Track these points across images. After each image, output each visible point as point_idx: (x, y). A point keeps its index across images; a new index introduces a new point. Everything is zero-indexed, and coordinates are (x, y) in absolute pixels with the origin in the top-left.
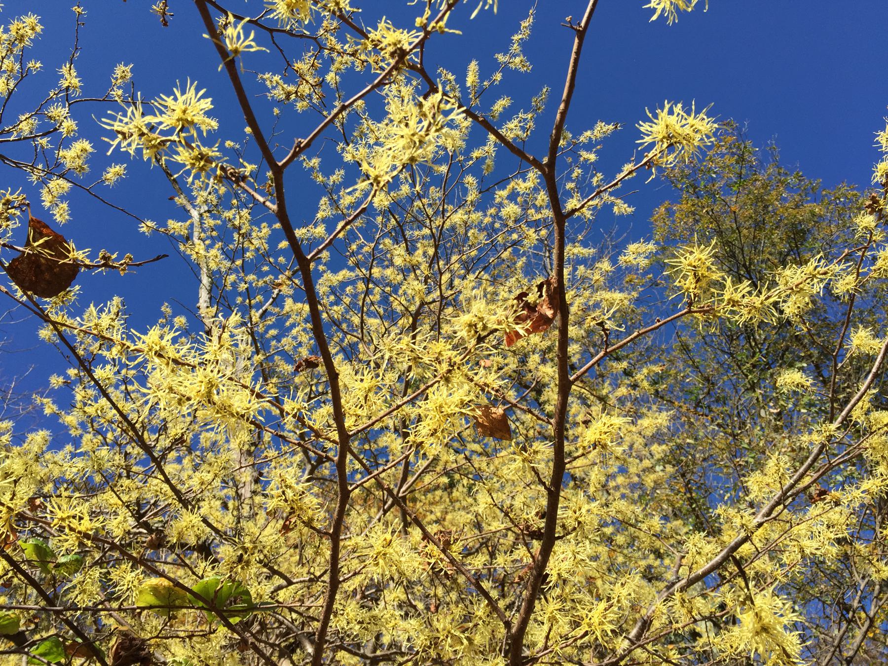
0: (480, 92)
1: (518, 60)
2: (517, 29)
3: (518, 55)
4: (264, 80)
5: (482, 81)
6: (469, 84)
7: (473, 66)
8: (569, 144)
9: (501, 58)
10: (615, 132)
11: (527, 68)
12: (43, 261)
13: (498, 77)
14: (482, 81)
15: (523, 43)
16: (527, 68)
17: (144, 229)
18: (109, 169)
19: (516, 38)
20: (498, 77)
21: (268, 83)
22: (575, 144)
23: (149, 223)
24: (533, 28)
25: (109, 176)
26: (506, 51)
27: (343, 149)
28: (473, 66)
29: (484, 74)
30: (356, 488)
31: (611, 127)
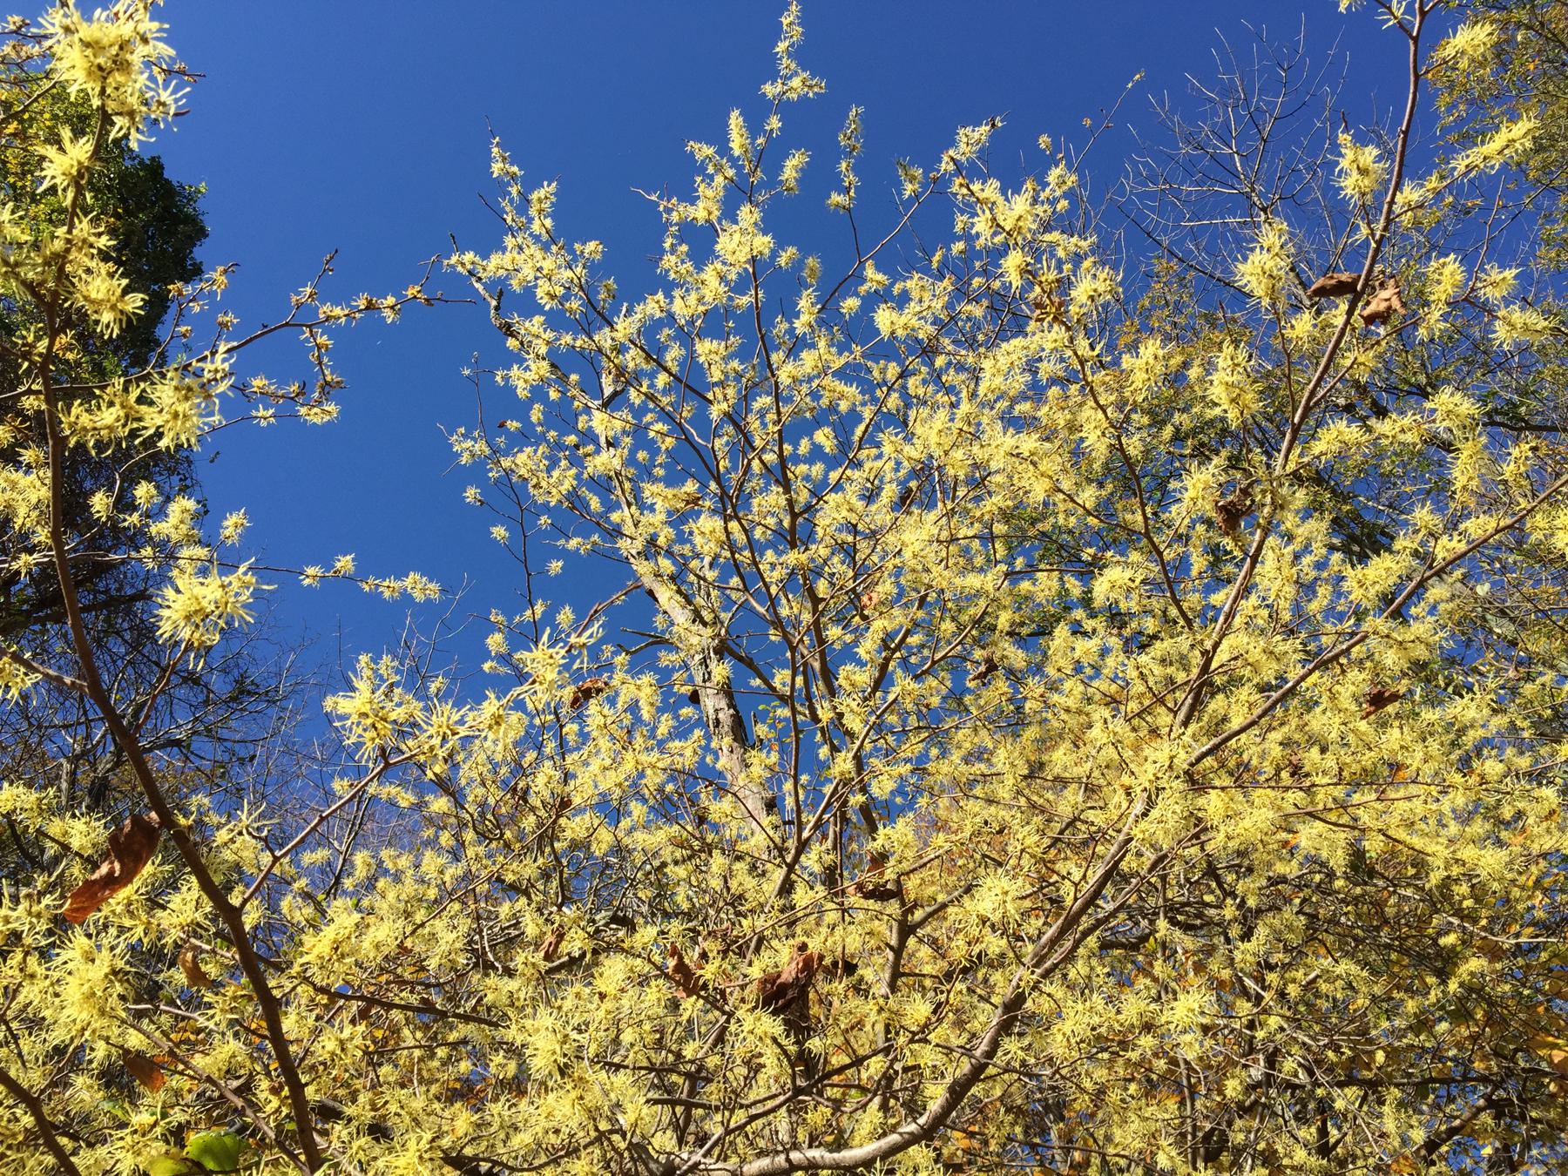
0: (760, 157)
1: (796, 82)
2: (777, 33)
3: (796, 74)
4: (453, 266)
5: (754, 139)
6: (737, 152)
7: (735, 120)
8: (924, 186)
9: (770, 90)
10: (995, 135)
11: (819, 87)
12: (744, 301)
13: (774, 123)
14: (754, 139)
15: (796, 53)
16: (819, 87)
17: (307, 582)
18: (226, 523)
19: (782, 46)
20: (774, 123)
21: (460, 269)
22: (935, 180)
23: (311, 571)
24: (803, 20)
25: (227, 533)
26: (773, 76)
27: (506, 379)
28: (735, 120)
29: (754, 126)
30: (1146, 518)
31: (985, 129)
